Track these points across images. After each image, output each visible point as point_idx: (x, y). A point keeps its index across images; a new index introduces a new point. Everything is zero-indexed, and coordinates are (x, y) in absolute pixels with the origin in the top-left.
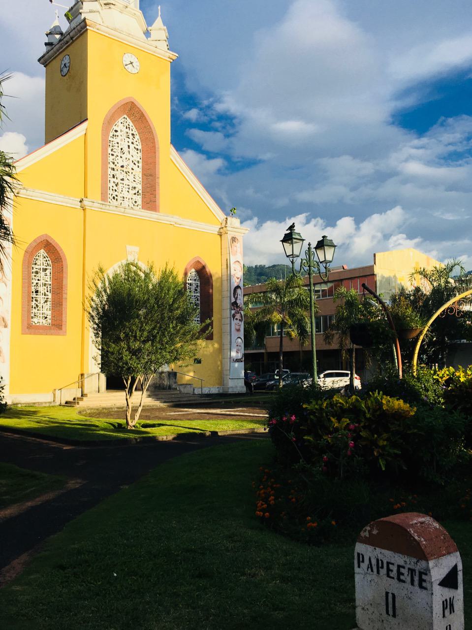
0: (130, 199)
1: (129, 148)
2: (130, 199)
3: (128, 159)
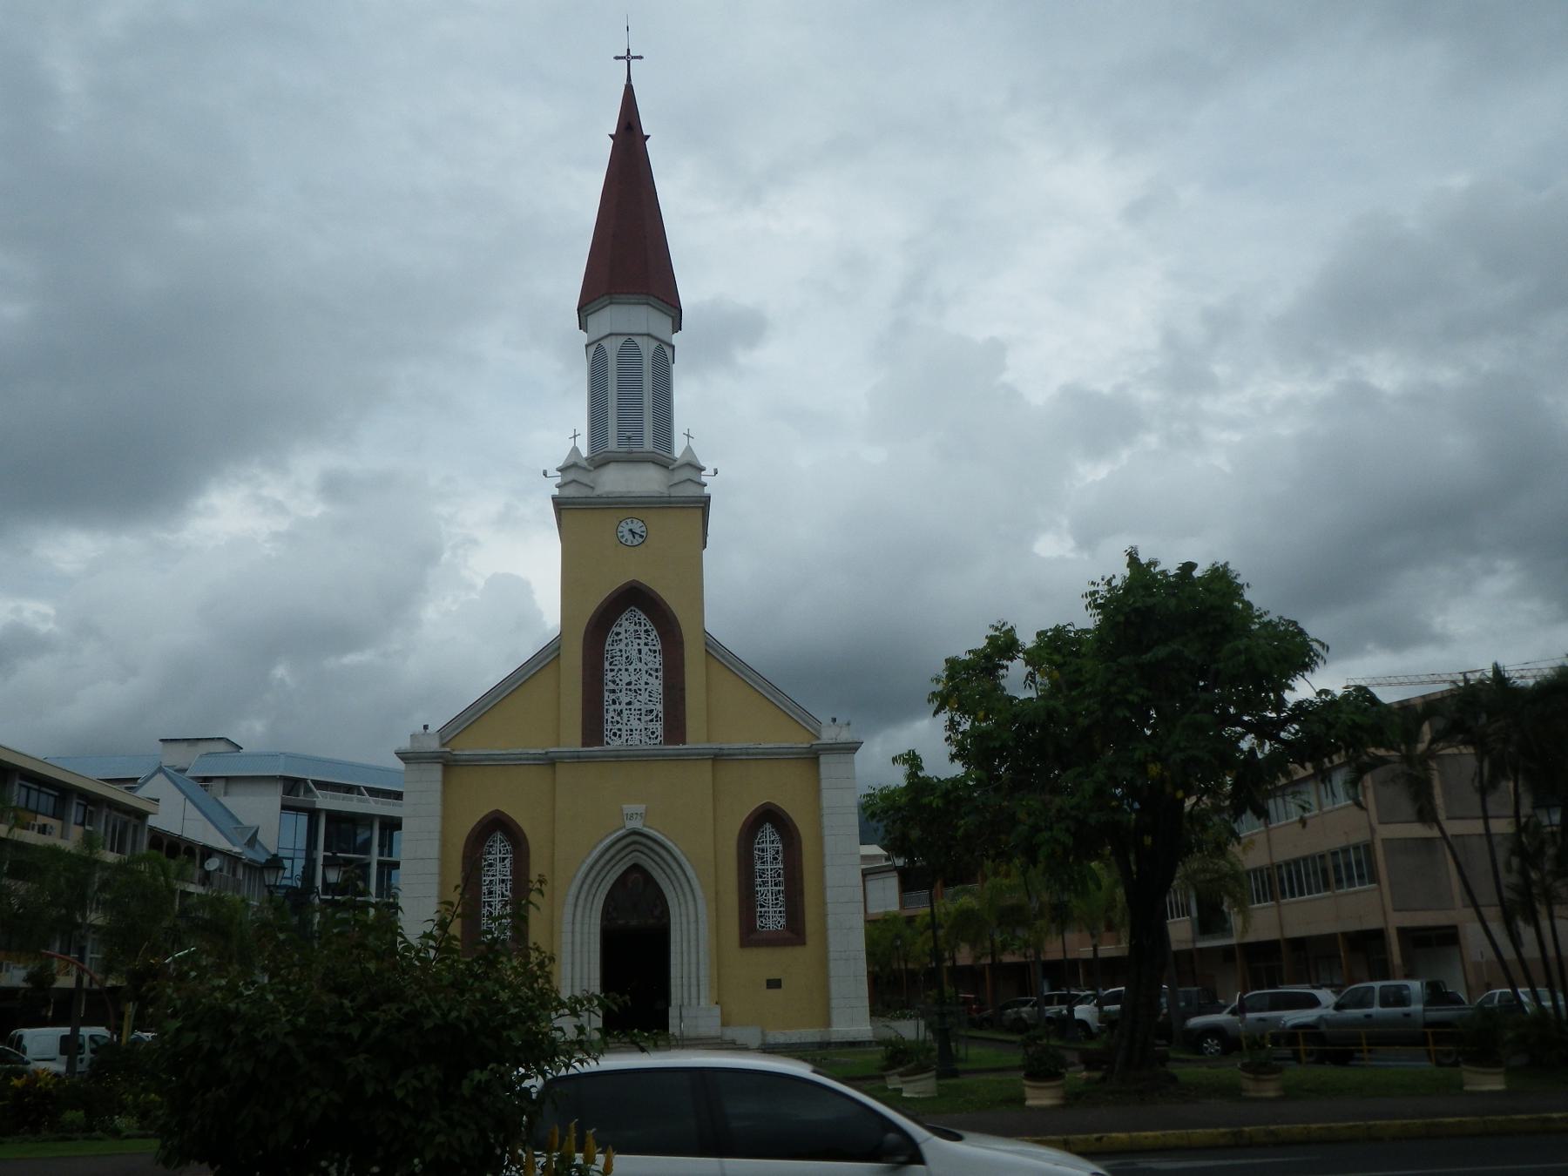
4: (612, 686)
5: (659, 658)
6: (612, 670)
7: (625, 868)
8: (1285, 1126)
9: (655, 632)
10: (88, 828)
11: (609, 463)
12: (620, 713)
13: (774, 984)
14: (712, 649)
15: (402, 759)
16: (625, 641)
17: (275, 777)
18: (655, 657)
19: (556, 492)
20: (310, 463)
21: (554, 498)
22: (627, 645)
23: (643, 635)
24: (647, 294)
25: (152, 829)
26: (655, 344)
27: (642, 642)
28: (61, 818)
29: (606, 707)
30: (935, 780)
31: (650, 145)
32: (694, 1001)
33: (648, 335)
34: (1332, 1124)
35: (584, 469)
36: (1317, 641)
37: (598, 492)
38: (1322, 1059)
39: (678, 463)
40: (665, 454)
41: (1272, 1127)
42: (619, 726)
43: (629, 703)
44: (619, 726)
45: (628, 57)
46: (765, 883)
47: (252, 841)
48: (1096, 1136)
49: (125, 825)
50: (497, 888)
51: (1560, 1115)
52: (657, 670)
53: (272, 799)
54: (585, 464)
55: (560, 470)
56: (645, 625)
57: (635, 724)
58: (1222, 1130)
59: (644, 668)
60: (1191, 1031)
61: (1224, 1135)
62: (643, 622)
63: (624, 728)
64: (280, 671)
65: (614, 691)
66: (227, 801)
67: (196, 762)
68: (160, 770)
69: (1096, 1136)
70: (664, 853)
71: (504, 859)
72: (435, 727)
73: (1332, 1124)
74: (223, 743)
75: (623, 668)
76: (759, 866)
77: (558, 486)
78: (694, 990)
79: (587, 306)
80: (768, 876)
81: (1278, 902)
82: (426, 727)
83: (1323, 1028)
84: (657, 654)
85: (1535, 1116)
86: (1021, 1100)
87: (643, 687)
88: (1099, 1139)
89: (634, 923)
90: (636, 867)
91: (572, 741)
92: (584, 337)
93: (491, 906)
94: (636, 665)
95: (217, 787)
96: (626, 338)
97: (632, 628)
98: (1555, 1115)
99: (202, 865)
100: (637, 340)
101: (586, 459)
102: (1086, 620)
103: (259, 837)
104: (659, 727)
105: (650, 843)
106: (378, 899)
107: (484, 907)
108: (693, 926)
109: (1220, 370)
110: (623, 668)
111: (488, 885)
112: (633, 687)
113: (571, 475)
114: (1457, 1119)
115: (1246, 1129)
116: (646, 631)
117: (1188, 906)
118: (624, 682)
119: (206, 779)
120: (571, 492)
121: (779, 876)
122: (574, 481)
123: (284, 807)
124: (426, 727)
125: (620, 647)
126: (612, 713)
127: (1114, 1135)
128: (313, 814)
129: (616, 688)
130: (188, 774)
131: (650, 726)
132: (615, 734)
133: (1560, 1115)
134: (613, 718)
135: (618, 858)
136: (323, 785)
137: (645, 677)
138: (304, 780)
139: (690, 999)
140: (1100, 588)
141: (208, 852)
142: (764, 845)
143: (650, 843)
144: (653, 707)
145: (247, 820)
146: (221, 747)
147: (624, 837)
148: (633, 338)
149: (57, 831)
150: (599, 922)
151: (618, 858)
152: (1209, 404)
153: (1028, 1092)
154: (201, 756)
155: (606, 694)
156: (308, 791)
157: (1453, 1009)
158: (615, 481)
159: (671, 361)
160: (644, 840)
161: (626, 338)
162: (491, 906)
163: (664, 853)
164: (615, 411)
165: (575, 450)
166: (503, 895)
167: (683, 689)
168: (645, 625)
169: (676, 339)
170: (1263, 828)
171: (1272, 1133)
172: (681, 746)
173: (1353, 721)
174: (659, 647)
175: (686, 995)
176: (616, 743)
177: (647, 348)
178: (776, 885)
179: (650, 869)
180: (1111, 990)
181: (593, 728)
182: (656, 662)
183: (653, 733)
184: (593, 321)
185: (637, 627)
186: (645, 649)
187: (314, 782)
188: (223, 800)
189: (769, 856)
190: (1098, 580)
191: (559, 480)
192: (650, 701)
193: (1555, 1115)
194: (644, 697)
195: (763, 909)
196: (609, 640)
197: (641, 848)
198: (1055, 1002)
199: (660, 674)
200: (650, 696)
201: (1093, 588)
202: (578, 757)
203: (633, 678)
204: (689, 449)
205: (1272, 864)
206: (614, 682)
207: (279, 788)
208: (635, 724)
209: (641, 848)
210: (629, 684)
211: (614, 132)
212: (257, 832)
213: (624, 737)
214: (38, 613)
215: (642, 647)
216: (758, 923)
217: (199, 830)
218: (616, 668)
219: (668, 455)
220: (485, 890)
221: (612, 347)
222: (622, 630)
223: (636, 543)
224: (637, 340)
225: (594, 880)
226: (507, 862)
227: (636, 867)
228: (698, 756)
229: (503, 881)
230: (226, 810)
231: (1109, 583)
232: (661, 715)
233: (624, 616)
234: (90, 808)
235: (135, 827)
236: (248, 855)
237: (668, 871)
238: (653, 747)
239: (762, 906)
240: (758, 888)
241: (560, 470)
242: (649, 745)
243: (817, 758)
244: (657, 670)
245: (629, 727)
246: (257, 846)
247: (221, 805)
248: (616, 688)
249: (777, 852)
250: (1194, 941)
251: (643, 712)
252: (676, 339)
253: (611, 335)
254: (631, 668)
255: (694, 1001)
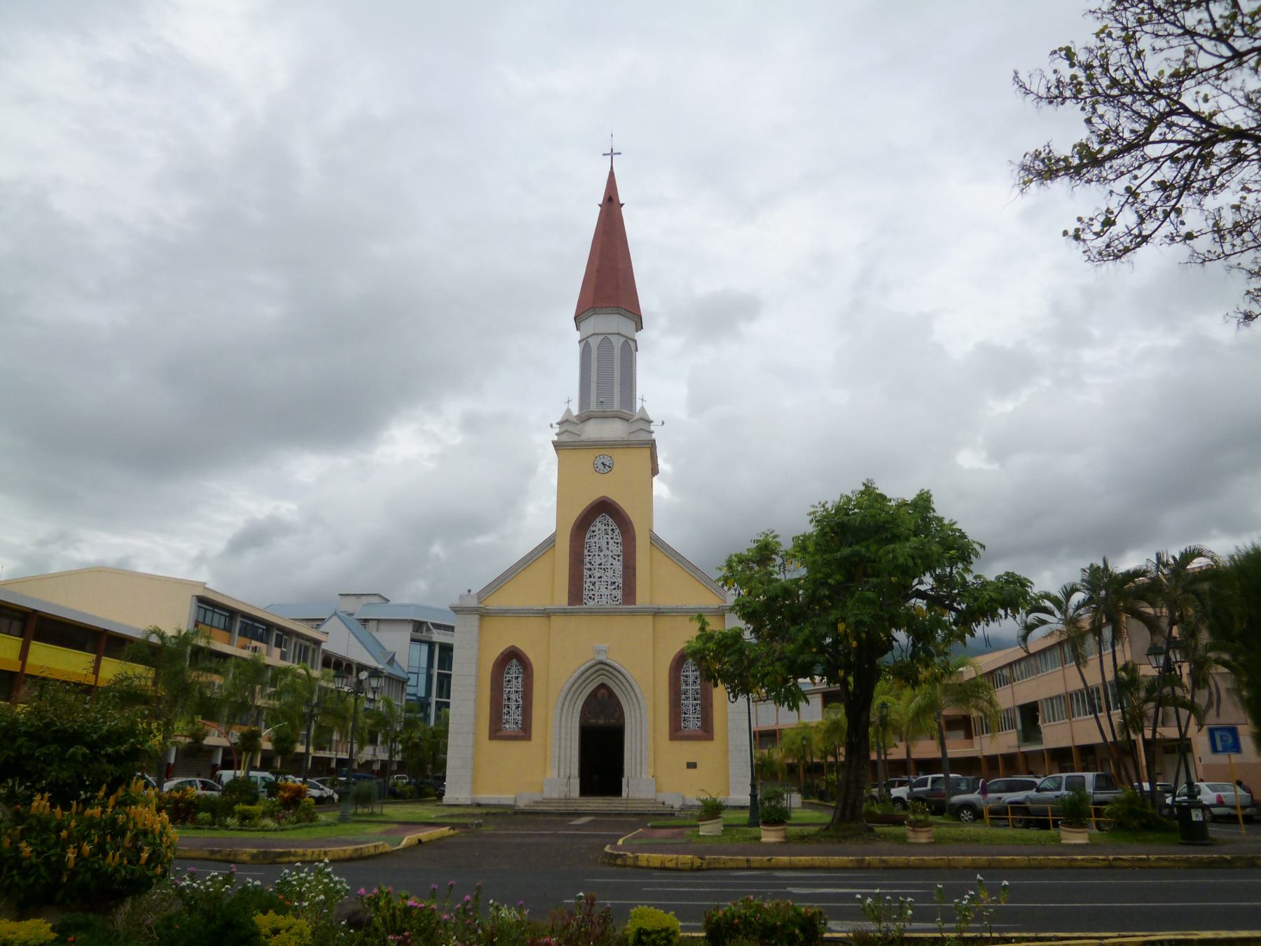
4: (589, 566)
5: (620, 548)
6: (589, 556)
7: (595, 686)
8: (893, 857)
9: (618, 531)
10: (283, 649)
11: (590, 418)
12: (594, 584)
13: (692, 765)
14: (655, 541)
15: (454, 611)
16: (598, 536)
17: (407, 620)
19: (556, 438)
20: (455, 407)
21: (553, 442)
22: (599, 539)
23: (610, 532)
24: (618, 307)
25: (324, 651)
26: (623, 340)
27: (609, 537)
28: (267, 643)
30: (154, 639)
32: (638, 775)
33: (618, 334)
34: (925, 858)
35: (575, 423)
36: (979, 543)
37: (583, 438)
38: (1028, 825)
39: (635, 418)
40: (627, 412)
41: (884, 858)
42: (593, 592)
43: (600, 577)
44: (593, 592)
45: (612, 154)
46: (687, 698)
47: (391, 661)
48: (767, 858)
49: (306, 648)
50: (513, 696)
51: (1082, 857)
52: (618, 556)
53: (406, 633)
54: (575, 420)
55: (558, 424)
57: (603, 591)
58: (850, 858)
59: (610, 554)
60: (953, 805)
61: (852, 860)
62: (610, 523)
63: (596, 594)
64: (437, 549)
65: (590, 569)
66: (377, 635)
67: (359, 609)
68: (335, 614)
69: (767, 858)
70: (620, 677)
71: (517, 678)
72: (475, 591)
73: (925, 858)
74: (377, 597)
75: (597, 554)
76: (683, 687)
77: (557, 434)
78: (638, 767)
79: (579, 318)
80: (690, 694)
81: (1070, 719)
82: (469, 591)
83: (1028, 804)
85: (1065, 857)
86: (758, 838)
87: (609, 567)
88: (770, 860)
89: (601, 722)
90: (603, 686)
91: (562, 600)
93: (509, 707)
94: (605, 552)
95: (372, 625)
96: (603, 336)
97: (603, 527)
98: (1079, 857)
99: (357, 676)
100: (611, 337)
101: (576, 416)
102: (810, 529)
103: (396, 658)
104: (619, 594)
105: (611, 670)
108: (638, 724)
109: (1097, 333)
110: (597, 554)
112: (602, 567)
113: (565, 427)
114: (1011, 857)
115: (867, 858)
116: (612, 530)
117: (1015, 722)
118: (597, 563)
119: (366, 621)
120: (565, 438)
121: (697, 693)
122: (567, 431)
123: (413, 640)
124: (469, 591)
125: (595, 540)
126: (588, 584)
127: (780, 858)
128: (431, 645)
129: (591, 567)
130: (355, 617)
131: (614, 593)
132: (590, 598)
133: (1082, 857)
135: (591, 679)
136: (438, 626)
137: (611, 560)
138: (426, 623)
139: (636, 772)
140: (818, 509)
141: (361, 667)
142: (688, 673)
143: (611, 670)
144: (615, 580)
145: (389, 647)
146: (376, 600)
147: (594, 665)
149: (264, 651)
150: (578, 719)
151: (591, 679)
152: (1088, 355)
153: (763, 833)
154: (363, 605)
155: (585, 571)
156: (428, 630)
157: (1111, 793)
158: (594, 431)
159: (633, 348)
160: (607, 668)
161: (603, 336)
162: (509, 707)
163: (620, 677)
164: (615, 379)
165: (569, 411)
166: (517, 701)
167: (634, 569)
170: (1061, 668)
171: (883, 861)
172: (632, 606)
173: (990, 596)
174: (620, 540)
175: (633, 771)
176: (591, 604)
177: (617, 342)
178: (695, 700)
179: (612, 687)
181: (576, 594)
182: (618, 550)
183: (615, 597)
184: (582, 325)
185: (606, 527)
186: (611, 542)
187: (433, 624)
188: (375, 634)
189: (691, 680)
190: (817, 504)
191: (557, 430)
193: (1079, 857)
194: (610, 573)
195: (686, 716)
196: (588, 536)
197: (606, 673)
198: (897, 785)
199: (621, 558)
201: (813, 510)
202: (590, 612)
203: (603, 561)
204: (643, 408)
205: (1067, 693)
206: (590, 563)
207: (410, 628)
208: (603, 591)
209: (606, 673)
210: (601, 564)
211: (601, 202)
212: (394, 655)
213: (596, 600)
214: (287, 509)
215: (609, 540)
216: (683, 725)
217: (356, 653)
218: (592, 554)
219: (630, 413)
220: (505, 697)
221: (594, 343)
222: (596, 529)
223: (606, 471)
224: (611, 337)
225: (575, 693)
226: (520, 680)
227: (603, 686)
228: (643, 612)
229: (517, 692)
230: (377, 641)
231: (823, 506)
232: (621, 585)
233: (598, 520)
234: (285, 637)
235: (314, 650)
236: (387, 670)
237: (624, 689)
238: (614, 606)
239: (685, 713)
240: (683, 702)
241: (558, 424)
242: (612, 605)
243: (723, 615)
244: (618, 556)
245: (599, 593)
246: (395, 664)
247: (374, 638)
248: (591, 567)
249: (696, 678)
250: (1019, 747)
251: (609, 583)
252: (639, 336)
253: (594, 334)
254: (602, 554)
255: (638, 775)
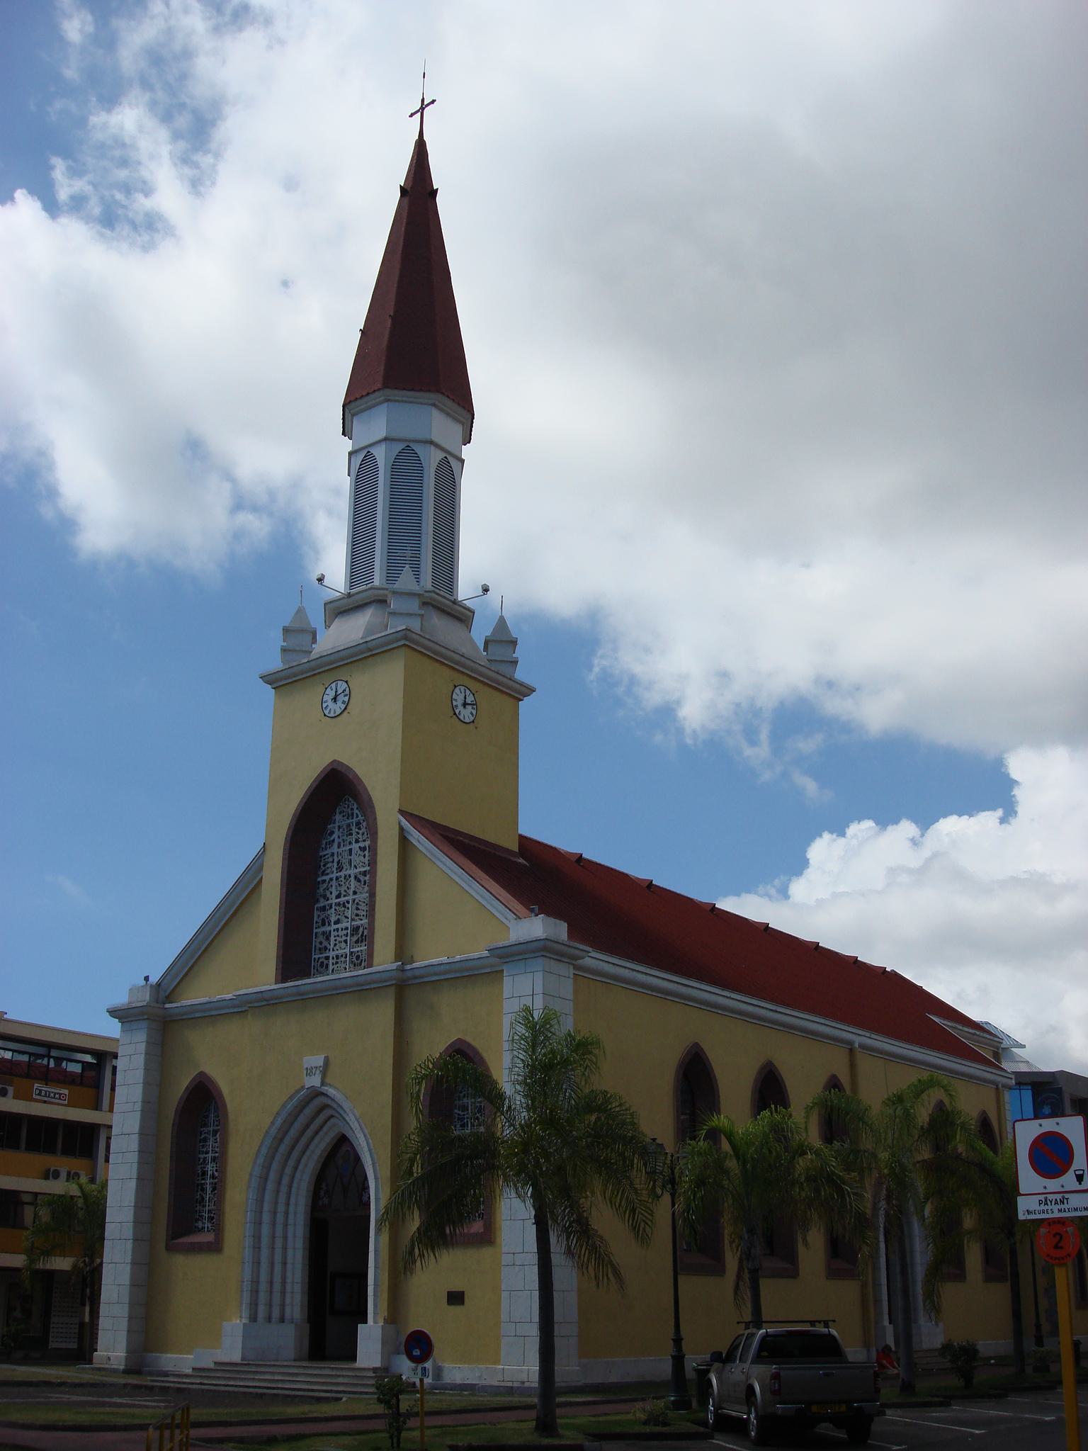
0: (358, 912)
1: (351, 855)
2: (358, 912)
3: (348, 877)
18: (364, 856)
29: (315, 931)
31: (439, 200)
56: (357, 817)
82: (147, 979)
84: (366, 852)
92: (347, 445)
96: (402, 446)
106: (596, 669)
107: (197, 1191)
111: (201, 1164)
124: (147, 979)
134: (321, 943)
148: (413, 446)
168: (357, 817)
169: (466, 452)
180: (977, 1432)
192: (357, 915)
200: (358, 909)
